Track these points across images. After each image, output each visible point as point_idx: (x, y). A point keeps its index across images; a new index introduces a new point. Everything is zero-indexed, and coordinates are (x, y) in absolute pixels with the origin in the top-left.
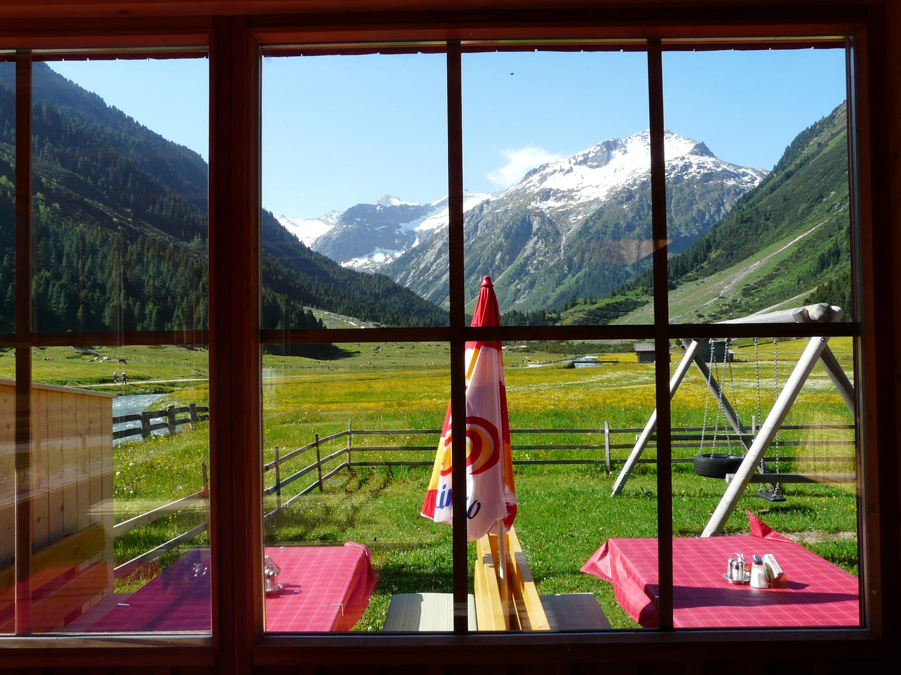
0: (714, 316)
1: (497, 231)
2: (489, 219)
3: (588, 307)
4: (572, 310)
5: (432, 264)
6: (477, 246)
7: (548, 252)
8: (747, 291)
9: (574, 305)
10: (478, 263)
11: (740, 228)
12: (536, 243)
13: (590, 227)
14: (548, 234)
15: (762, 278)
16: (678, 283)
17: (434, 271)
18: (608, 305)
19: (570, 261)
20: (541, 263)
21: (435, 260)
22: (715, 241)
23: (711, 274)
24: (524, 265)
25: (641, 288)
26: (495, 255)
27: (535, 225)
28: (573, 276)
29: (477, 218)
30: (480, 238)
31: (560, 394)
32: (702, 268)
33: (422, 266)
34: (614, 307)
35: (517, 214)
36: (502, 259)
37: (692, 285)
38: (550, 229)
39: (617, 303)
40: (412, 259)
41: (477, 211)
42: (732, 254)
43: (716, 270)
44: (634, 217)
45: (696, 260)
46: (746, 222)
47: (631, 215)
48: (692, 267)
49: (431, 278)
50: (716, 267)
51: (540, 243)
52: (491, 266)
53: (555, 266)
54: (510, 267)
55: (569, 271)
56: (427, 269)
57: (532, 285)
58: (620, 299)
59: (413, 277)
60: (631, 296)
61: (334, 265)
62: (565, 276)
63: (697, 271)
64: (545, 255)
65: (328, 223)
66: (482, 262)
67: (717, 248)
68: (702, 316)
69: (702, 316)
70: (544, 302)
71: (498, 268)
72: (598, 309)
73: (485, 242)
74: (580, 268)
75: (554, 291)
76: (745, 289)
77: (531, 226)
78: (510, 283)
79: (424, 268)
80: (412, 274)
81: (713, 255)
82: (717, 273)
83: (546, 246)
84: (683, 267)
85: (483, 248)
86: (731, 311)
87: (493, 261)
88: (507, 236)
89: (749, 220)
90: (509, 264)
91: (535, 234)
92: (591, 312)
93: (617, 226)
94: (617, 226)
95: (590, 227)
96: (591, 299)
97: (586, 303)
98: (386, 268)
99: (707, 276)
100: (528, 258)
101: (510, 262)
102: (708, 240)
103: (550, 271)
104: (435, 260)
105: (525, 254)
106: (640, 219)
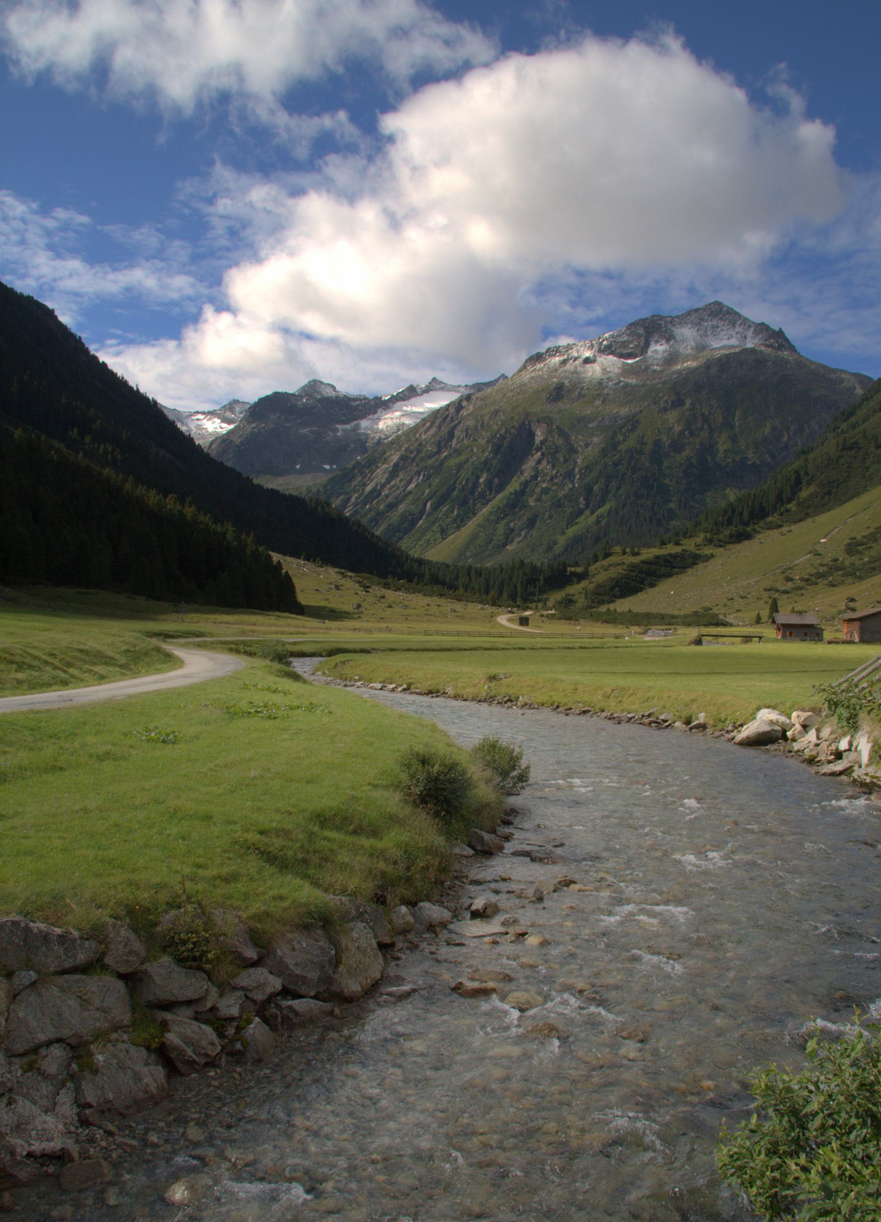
0: (807, 580)
1: (482, 442)
2: (471, 423)
3: (630, 560)
4: (605, 562)
5: (383, 486)
6: (453, 462)
7: (556, 476)
8: (852, 548)
9: (607, 555)
10: (453, 488)
11: (841, 457)
12: (539, 462)
13: (619, 443)
14: (557, 450)
15: (872, 530)
16: (754, 530)
17: (387, 496)
18: (657, 557)
19: (589, 490)
20: (546, 491)
21: (388, 481)
22: (807, 474)
23: (800, 520)
24: (521, 494)
25: (702, 535)
26: (478, 478)
27: (539, 436)
28: (592, 513)
29: (452, 420)
30: (455, 451)
31: (687, 632)
32: (788, 511)
33: (368, 489)
34: (666, 561)
35: (512, 418)
36: (489, 483)
37: (775, 533)
38: (560, 442)
39: (670, 555)
40: (354, 477)
41: (452, 410)
42: (829, 493)
43: (807, 516)
44: (682, 432)
45: (780, 499)
46: (850, 448)
47: (678, 429)
48: (775, 509)
49: (382, 507)
50: (808, 511)
51: (545, 463)
52: (472, 493)
53: (565, 497)
54: (500, 496)
55: (587, 505)
56: (375, 493)
57: (531, 523)
58: (672, 549)
59: (356, 504)
60: (689, 545)
61: (249, 481)
62: (580, 512)
63: (781, 514)
64: (552, 479)
65: (229, 421)
66: (458, 486)
67: (809, 483)
68: (791, 580)
69: (791, 580)
70: (549, 549)
71: (482, 496)
72: (643, 562)
73: (463, 458)
74: (602, 502)
75: (564, 533)
76: (849, 544)
77: (532, 435)
78: (499, 520)
79: (371, 492)
80: (353, 500)
81: (804, 494)
82: (809, 520)
83: (553, 467)
84: (762, 508)
85: (460, 467)
86: (831, 574)
87: (476, 484)
88: (497, 449)
89: (854, 446)
90: (499, 491)
91: (538, 449)
92: (633, 567)
93: (657, 444)
94: (657, 444)
95: (619, 443)
96: (633, 548)
97: (624, 553)
98: (314, 490)
99: (795, 522)
100: (526, 484)
101: (501, 488)
102: (797, 472)
103: (558, 504)
104: (388, 481)
105: (522, 479)
106: (692, 434)
